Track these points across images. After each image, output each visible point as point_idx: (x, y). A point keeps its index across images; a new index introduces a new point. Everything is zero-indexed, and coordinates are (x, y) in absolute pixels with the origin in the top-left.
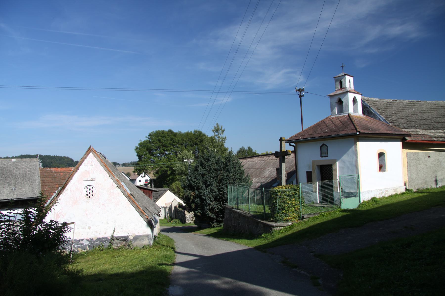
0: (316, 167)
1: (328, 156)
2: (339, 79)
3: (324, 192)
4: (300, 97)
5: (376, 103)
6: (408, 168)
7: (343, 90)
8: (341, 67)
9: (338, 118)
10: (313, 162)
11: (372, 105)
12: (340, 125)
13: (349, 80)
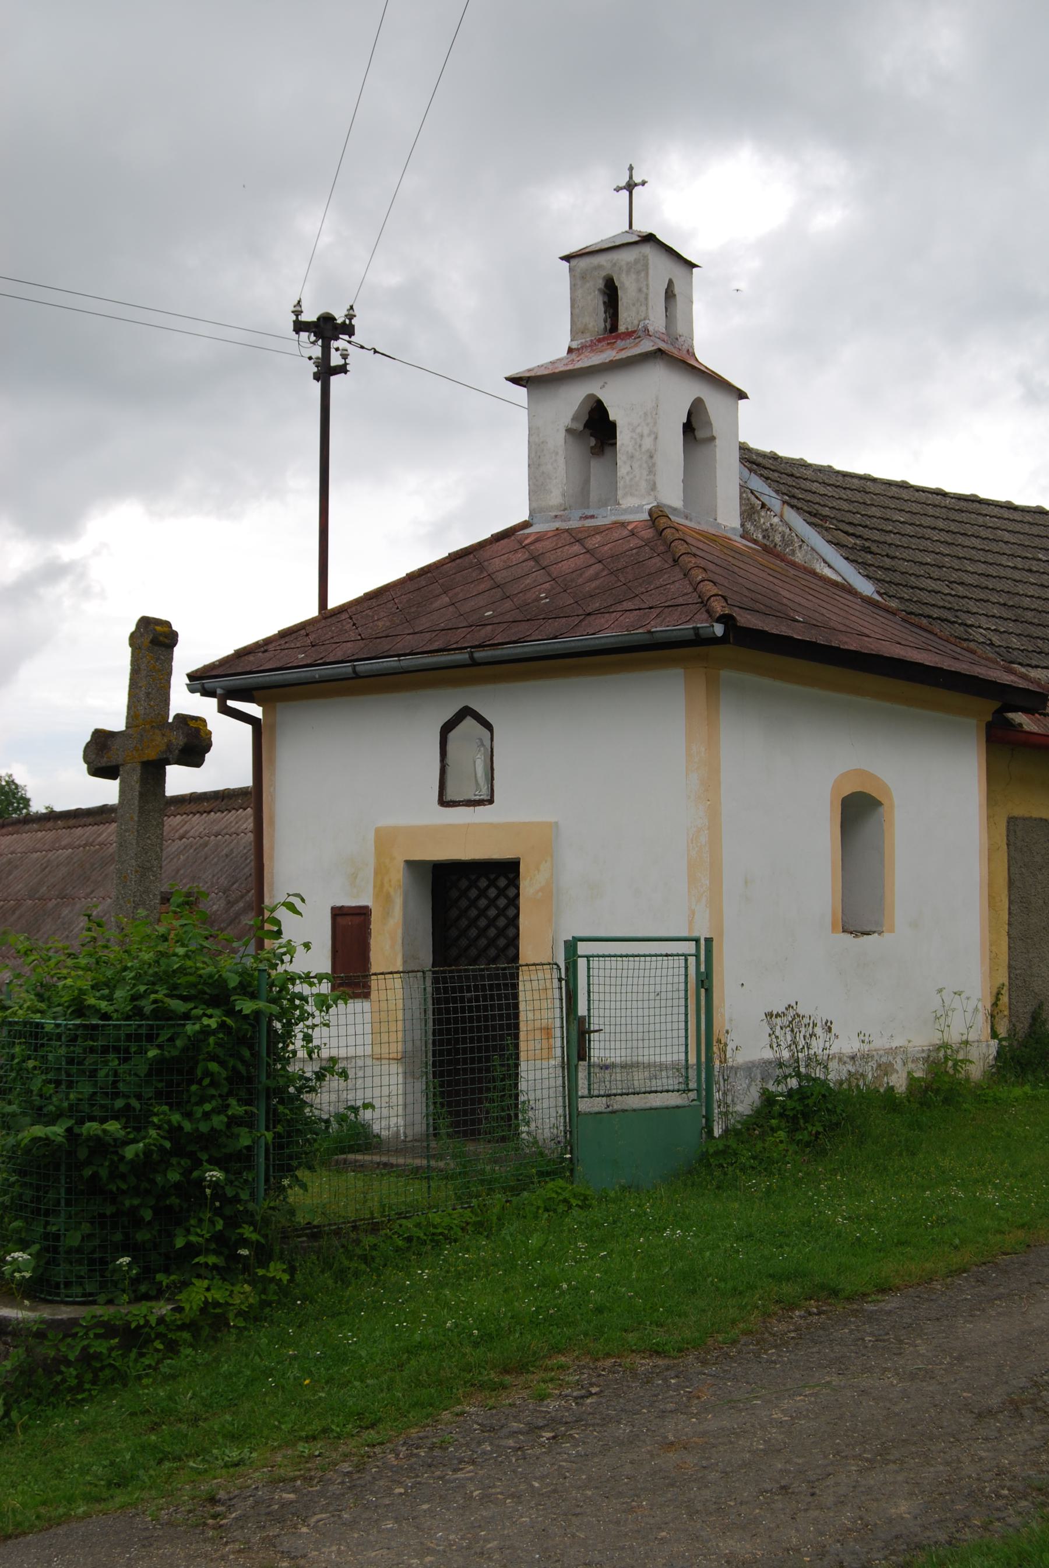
0: (397, 874)
1: (491, 801)
2: (599, 267)
3: (449, 1053)
4: (325, 372)
5: (822, 490)
6: (1010, 924)
7: (620, 344)
8: (618, 189)
9: (580, 536)
10: (384, 839)
11: (799, 499)
12: (591, 580)
13: (671, 283)
